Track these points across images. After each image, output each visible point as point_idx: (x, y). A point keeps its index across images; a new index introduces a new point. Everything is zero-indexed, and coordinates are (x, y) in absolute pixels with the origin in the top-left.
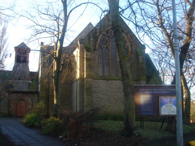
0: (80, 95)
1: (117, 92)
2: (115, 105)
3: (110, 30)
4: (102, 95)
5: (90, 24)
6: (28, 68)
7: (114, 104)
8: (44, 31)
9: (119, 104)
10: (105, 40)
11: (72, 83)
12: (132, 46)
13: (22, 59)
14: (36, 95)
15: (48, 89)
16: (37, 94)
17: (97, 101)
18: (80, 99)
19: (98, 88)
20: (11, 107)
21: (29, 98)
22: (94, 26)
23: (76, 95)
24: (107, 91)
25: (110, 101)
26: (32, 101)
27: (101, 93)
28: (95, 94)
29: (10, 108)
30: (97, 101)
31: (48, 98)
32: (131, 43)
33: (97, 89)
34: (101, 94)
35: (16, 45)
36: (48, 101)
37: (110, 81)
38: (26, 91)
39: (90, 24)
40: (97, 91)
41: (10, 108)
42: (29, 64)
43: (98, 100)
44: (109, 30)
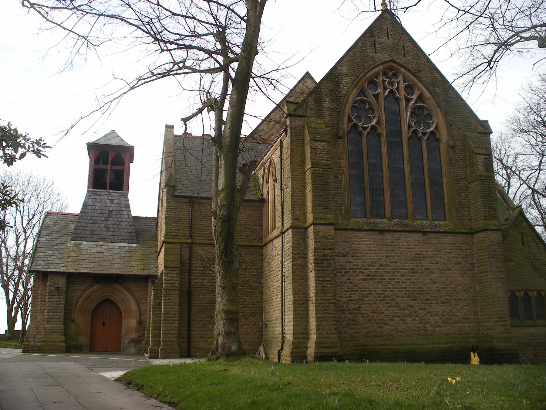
0: (293, 279)
1: (411, 269)
2: (406, 312)
3: (381, 77)
4: (365, 279)
5: (308, 75)
6: (128, 207)
7: (404, 310)
8: (181, 65)
9: (421, 309)
10: (367, 107)
11: (262, 247)
12: (449, 126)
13: (109, 177)
14: (150, 284)
15: (190, 263)
16: (153, 283)
17: (352, 300)
18: (294, 294)
19: (351, 259)
20: (73, 321)
21: (128, 294)
22: (318, 79)
23: (279, 284)
24: (381, 265)
25: (392, 300)
26: (138, 303)
27: (362, 272)
28: (343, 276)
29: (73, 325)
30: (352, 300)
31: (189, 293)
32: (446, 114)
33: (350, 262)
34: (362, 276)
35: (93, 139)
36: (189, 300)
37: (388, 236)
38: (506, 364)
39: (308, 75)
40: (347, 266)
41: (73, 325)
42: (139, 216)
43: (354, 297)
44: (377, 75)
